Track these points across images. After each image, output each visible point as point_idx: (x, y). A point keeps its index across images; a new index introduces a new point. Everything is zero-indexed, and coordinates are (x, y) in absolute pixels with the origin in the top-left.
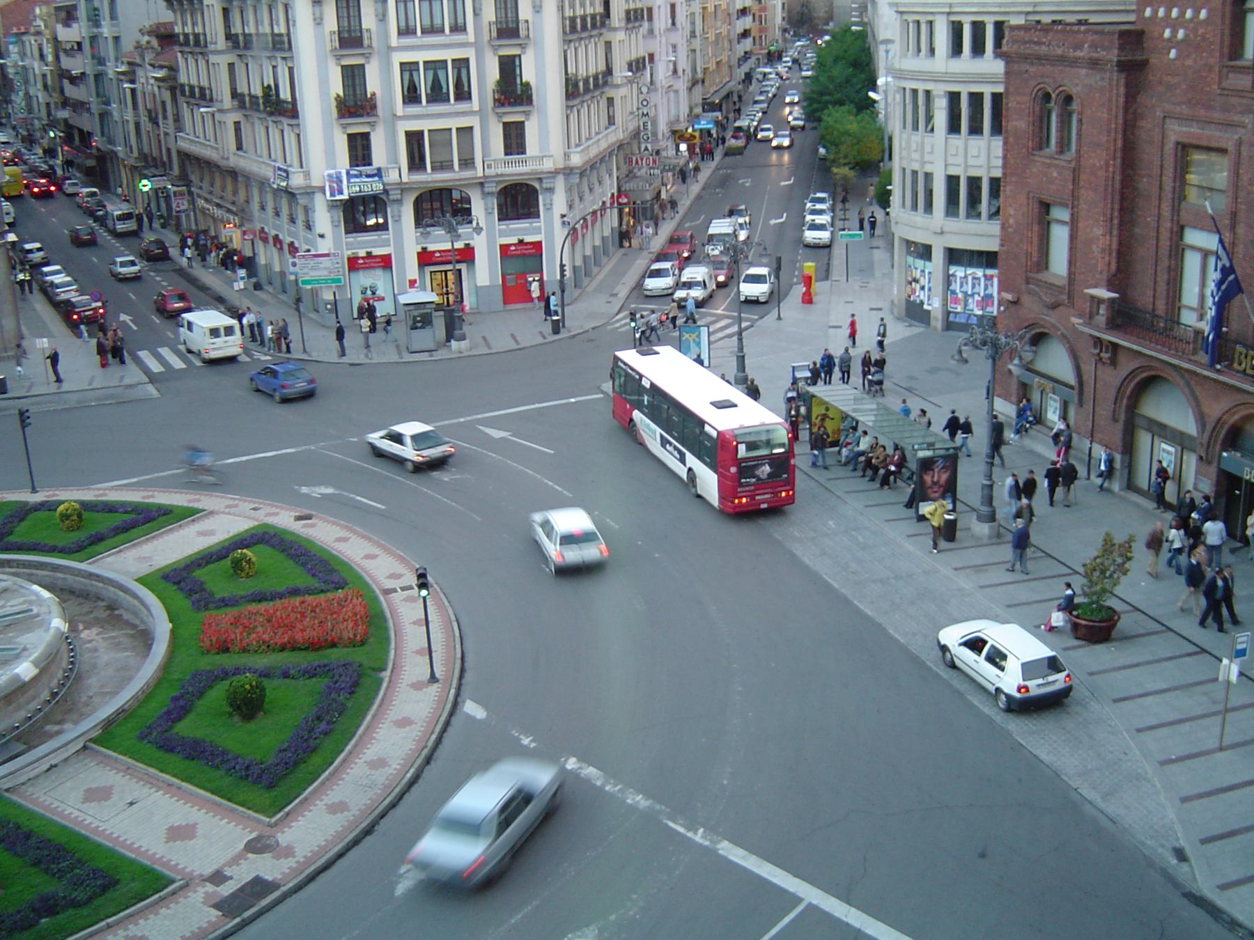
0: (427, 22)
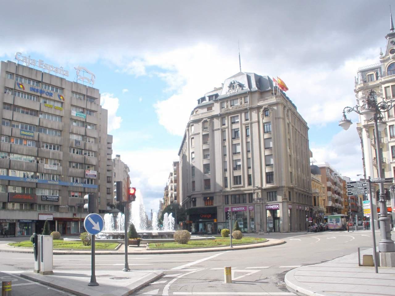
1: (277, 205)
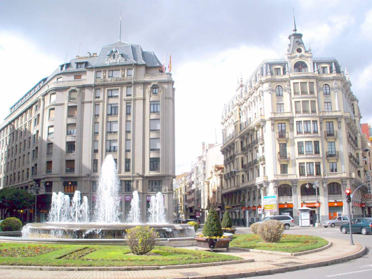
0: (306, 130)
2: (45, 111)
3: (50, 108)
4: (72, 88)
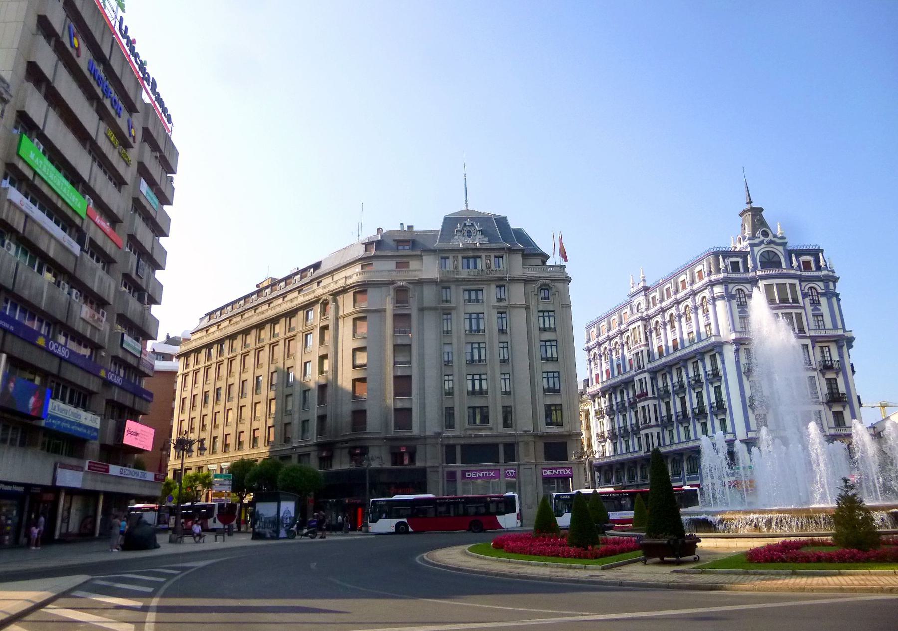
1: (568, 468)
2: (340, 321)
3: (355, 316)
4: (400, 284)
